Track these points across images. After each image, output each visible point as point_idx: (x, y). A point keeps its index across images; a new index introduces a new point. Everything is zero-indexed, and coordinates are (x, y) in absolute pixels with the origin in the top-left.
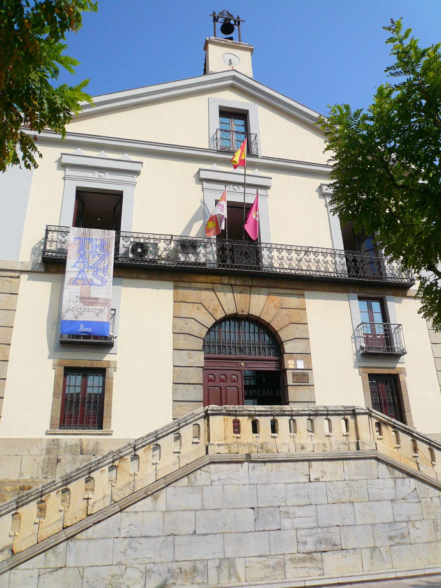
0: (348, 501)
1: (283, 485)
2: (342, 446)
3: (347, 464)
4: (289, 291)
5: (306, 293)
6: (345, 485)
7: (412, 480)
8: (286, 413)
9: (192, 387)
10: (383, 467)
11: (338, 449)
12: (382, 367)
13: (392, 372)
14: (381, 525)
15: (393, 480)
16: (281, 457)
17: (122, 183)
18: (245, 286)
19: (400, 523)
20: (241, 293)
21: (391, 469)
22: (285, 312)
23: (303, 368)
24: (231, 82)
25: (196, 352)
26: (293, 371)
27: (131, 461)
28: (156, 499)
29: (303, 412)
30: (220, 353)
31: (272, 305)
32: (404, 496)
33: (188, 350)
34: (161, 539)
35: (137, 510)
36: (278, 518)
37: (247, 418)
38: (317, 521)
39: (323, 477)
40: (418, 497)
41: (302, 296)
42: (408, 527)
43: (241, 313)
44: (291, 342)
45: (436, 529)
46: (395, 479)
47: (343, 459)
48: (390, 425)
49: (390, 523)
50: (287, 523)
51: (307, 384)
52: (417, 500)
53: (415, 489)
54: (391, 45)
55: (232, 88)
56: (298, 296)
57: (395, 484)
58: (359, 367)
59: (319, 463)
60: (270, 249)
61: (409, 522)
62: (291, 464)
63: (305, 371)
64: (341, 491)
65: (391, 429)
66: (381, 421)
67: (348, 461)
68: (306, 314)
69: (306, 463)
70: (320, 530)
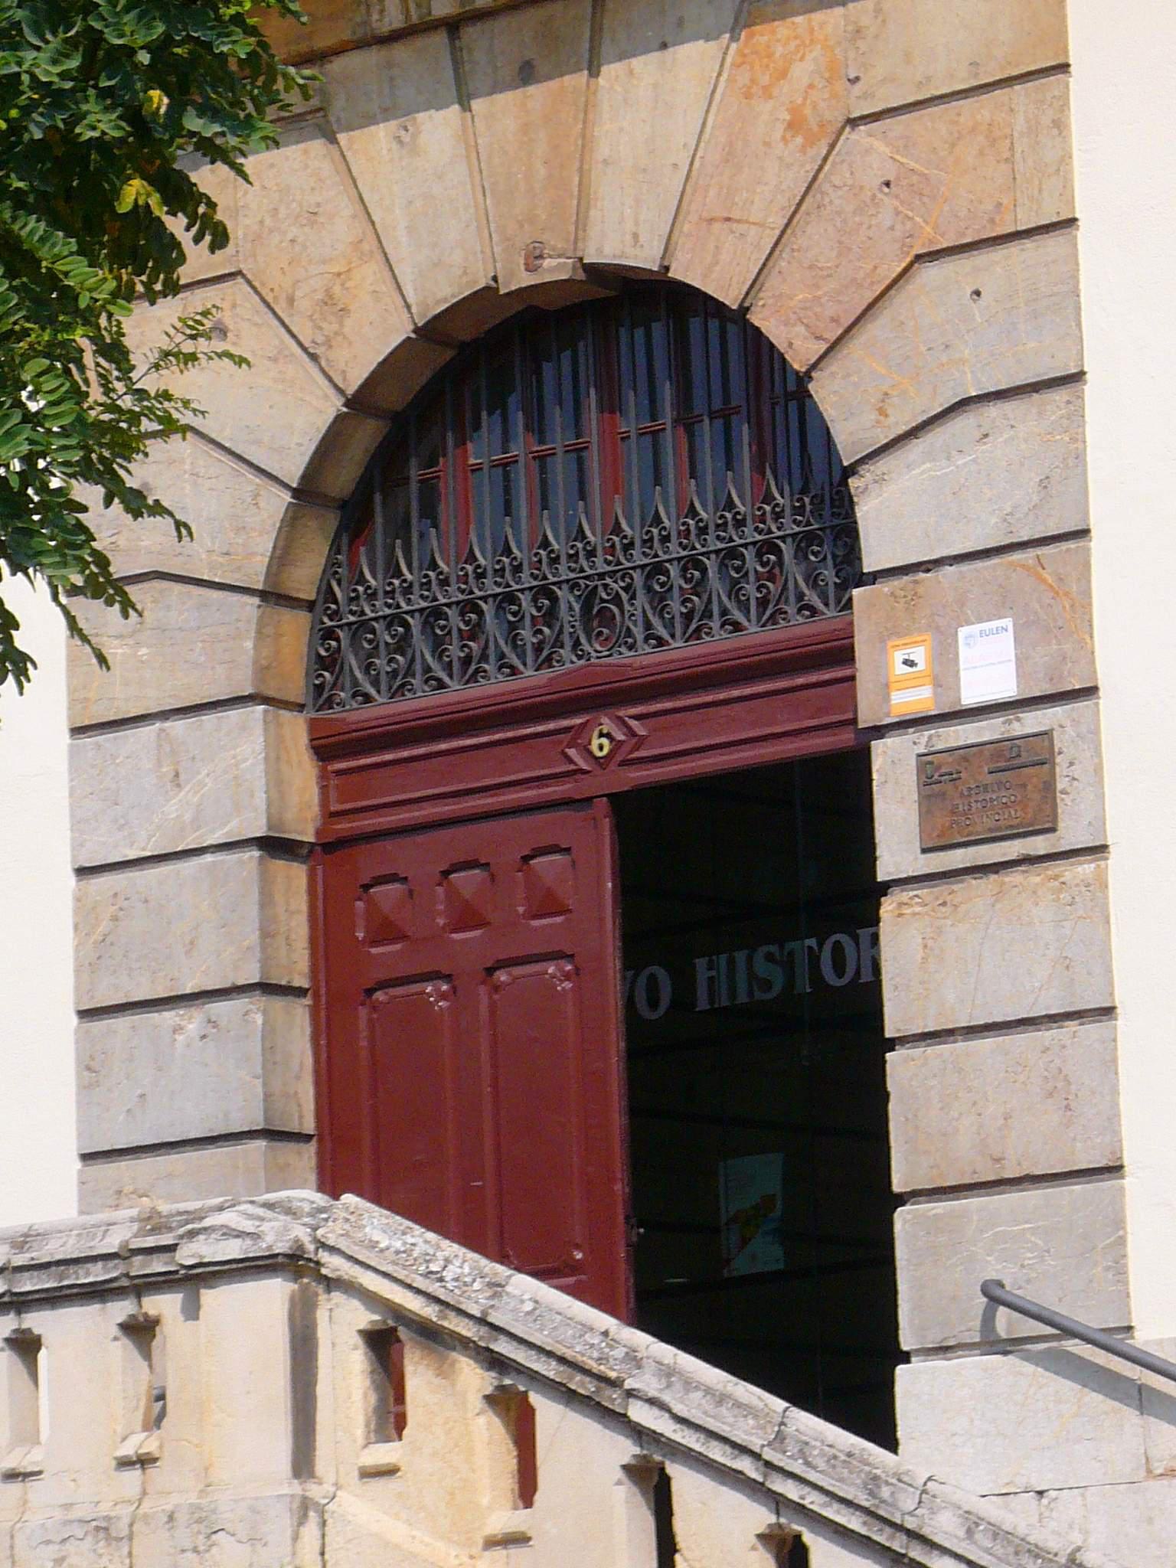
9: (192, 1021)
20: (527, 74)
22: (872, 153)
25: (209, 719)
27: (890, 1443)
30: (694, 625)
31: (769, 117)
33: (165, 715)
44: (916, 448)
48: (465, 1344)
51: (1039, 845)
63: (1031, 722)
68: (1060, 125)
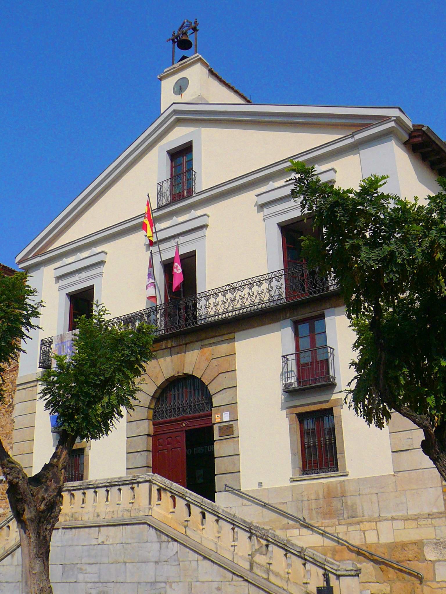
0: (122, 561)
1: (80, 547)
2: (125, 513)
3: (125, 528)
4: (220, 339)
5: (237, 335)
6: (121, 547)
7: (175, 543)
8: (90, 486)
9: (139, 454)
10: (153, 532)
11: (123, 515)
12: (311, 403)
13: (324, 406)
14: (145, 584)
15: (159, 543)
16: (80, 524)
17: (87, 279)
18: (180, 345)
19: (160, 584)
20: (178, 353)
21: (159, 533)
22: (215, 362)
23: (229, 420)
24: (174, 117)
26: (219, 425)
28: (13, 557)
29: (101, 485)
30: (170, 416)
32: (166, 560)
34: (14, 584)
35: (4, 564)
36: (76, 573)
37: (67, 492)
38: (99, 577)
39: (107, 540)
40: (178, 560)
41: (233, 340)
42: (165, 587)
43: (177, 375)
45: (190, 592)
46: (161, 542)
47: (122, 525)
48: (168, 491)
49: (152, 582)
50: (81, 577)
52: (177, 563)
53: (177, 552)
54: (193, 22)
55: (179, 122)
56: (228, 341)
57: (160, 548)
58: (287, 408)
59: (106, 528)
60: (207, 297)
61: (167, 583)
62: (87, 530)
63: (231, 423)
64: (118, 552)
65: (169, 494)
66: (161, 487)
67: (126, 526)
69: (97, 529)
70: (100, 585)
